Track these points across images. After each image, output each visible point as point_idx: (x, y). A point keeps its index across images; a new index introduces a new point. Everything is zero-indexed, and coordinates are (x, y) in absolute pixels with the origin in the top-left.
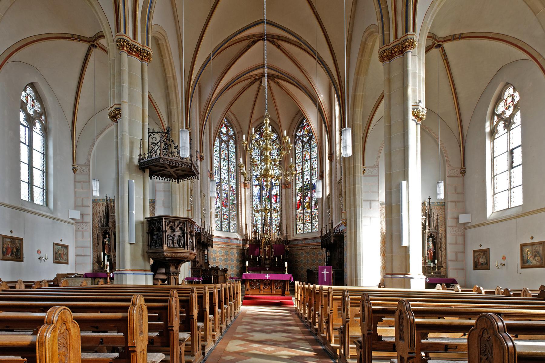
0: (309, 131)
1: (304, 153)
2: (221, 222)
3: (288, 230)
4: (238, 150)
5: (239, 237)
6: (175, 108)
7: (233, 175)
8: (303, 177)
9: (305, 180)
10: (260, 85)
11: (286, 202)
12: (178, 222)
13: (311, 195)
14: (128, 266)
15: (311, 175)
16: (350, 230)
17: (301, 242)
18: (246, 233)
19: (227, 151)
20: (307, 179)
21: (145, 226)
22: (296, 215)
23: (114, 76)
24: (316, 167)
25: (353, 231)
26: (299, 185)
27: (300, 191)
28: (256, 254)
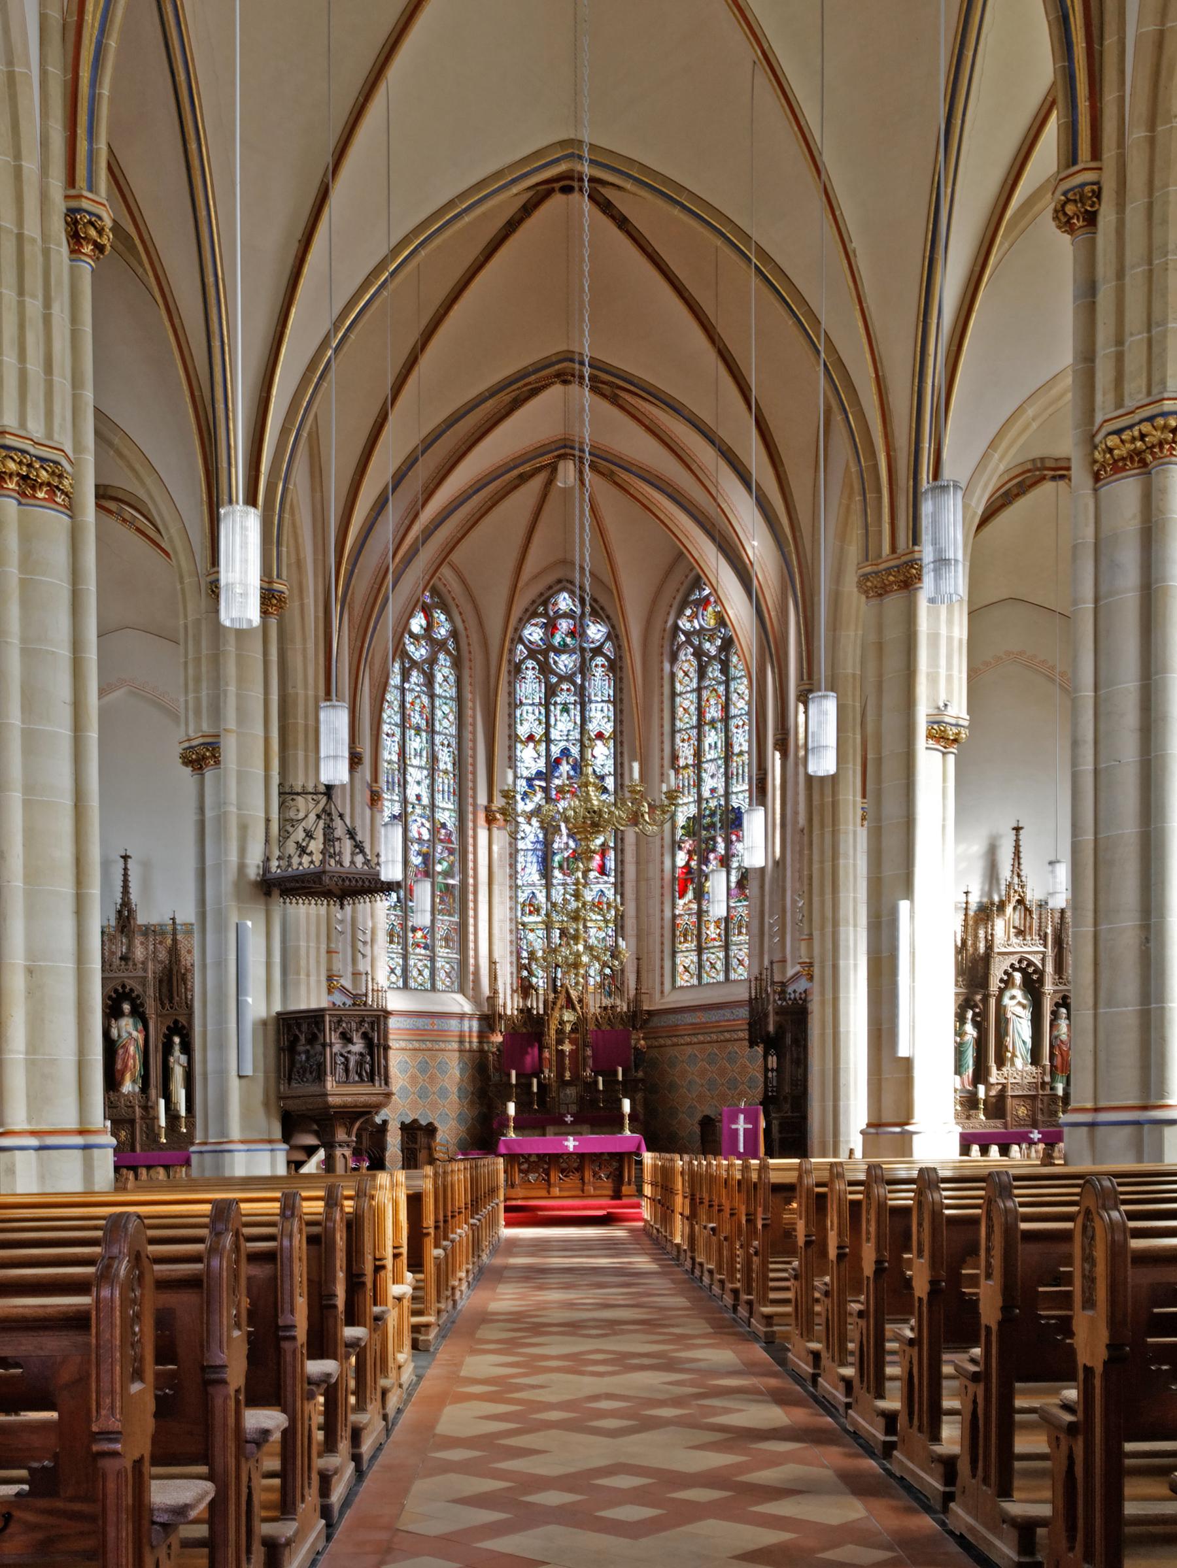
0: (721, 621)
1: (705, 694)
2: (405, 957)
3: (644, 975)
4: (467, 689)
5: (467, 1007)
6: (299, 646)
7: (445, 782)
8: (699, 783)
9: (706, 794)
10: (550, 482)
11: (638, 872)
12: (358, 1020)
13: (727, 848)
14: (235, 1132)
15: (728, 777)
16: (823, 993)
17: (689, 1018)
18: (495, 991)
19: (425, 700)
20: (713, 790)
21: (271, 1029)
22: (674, 917)
23: (198, 660)
24: (745, 748)
25: (829, 996)
26: (685, 811)
27: (688, 834)
28: (528, 1070)
